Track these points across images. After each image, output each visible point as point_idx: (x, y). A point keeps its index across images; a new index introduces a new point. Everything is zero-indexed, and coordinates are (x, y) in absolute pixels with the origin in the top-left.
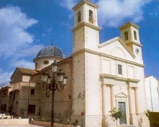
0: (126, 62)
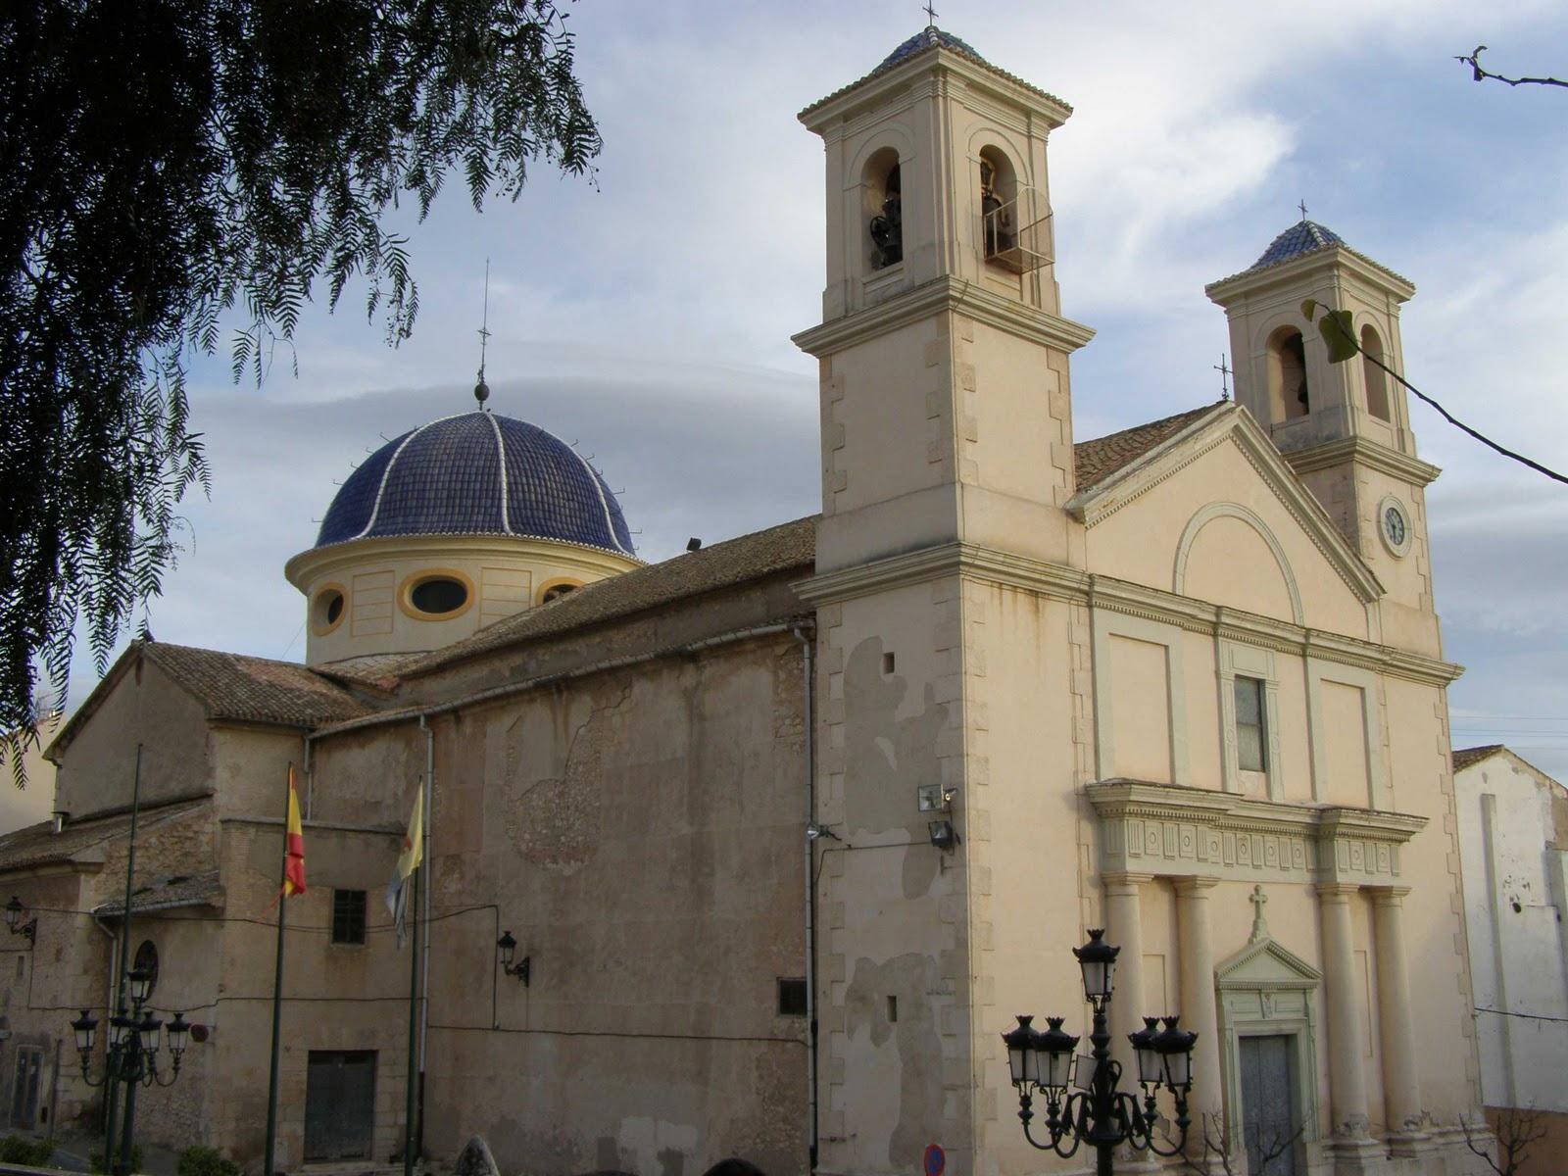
0: (1305, 645)
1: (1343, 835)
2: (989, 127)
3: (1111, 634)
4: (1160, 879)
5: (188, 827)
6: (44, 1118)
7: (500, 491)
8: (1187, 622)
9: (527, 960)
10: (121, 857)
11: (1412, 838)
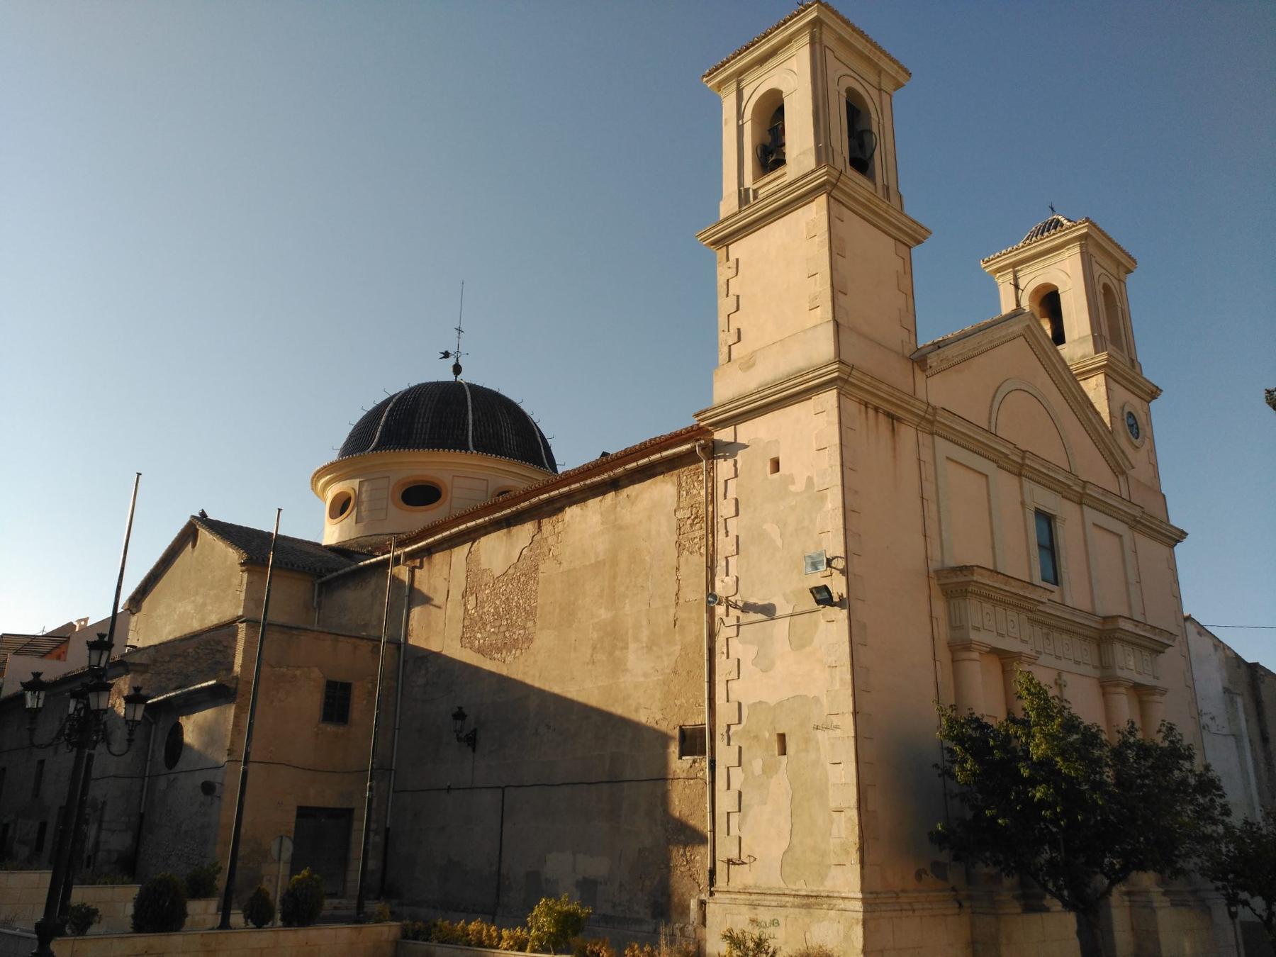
1: (1121, 640)
2: (849, 74)
3: (947, 458)
4: (995, 651)
5: (219, 643)
6: (89, 862)
7: (468, 425)
8: (1001, 461)
9: (475, 730)
10: (164, 662)
11: (1167, 650)
